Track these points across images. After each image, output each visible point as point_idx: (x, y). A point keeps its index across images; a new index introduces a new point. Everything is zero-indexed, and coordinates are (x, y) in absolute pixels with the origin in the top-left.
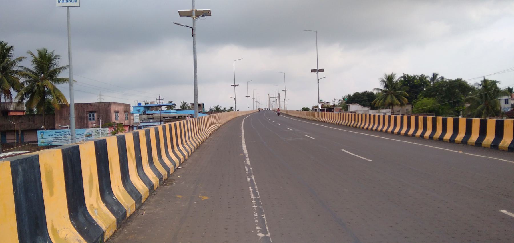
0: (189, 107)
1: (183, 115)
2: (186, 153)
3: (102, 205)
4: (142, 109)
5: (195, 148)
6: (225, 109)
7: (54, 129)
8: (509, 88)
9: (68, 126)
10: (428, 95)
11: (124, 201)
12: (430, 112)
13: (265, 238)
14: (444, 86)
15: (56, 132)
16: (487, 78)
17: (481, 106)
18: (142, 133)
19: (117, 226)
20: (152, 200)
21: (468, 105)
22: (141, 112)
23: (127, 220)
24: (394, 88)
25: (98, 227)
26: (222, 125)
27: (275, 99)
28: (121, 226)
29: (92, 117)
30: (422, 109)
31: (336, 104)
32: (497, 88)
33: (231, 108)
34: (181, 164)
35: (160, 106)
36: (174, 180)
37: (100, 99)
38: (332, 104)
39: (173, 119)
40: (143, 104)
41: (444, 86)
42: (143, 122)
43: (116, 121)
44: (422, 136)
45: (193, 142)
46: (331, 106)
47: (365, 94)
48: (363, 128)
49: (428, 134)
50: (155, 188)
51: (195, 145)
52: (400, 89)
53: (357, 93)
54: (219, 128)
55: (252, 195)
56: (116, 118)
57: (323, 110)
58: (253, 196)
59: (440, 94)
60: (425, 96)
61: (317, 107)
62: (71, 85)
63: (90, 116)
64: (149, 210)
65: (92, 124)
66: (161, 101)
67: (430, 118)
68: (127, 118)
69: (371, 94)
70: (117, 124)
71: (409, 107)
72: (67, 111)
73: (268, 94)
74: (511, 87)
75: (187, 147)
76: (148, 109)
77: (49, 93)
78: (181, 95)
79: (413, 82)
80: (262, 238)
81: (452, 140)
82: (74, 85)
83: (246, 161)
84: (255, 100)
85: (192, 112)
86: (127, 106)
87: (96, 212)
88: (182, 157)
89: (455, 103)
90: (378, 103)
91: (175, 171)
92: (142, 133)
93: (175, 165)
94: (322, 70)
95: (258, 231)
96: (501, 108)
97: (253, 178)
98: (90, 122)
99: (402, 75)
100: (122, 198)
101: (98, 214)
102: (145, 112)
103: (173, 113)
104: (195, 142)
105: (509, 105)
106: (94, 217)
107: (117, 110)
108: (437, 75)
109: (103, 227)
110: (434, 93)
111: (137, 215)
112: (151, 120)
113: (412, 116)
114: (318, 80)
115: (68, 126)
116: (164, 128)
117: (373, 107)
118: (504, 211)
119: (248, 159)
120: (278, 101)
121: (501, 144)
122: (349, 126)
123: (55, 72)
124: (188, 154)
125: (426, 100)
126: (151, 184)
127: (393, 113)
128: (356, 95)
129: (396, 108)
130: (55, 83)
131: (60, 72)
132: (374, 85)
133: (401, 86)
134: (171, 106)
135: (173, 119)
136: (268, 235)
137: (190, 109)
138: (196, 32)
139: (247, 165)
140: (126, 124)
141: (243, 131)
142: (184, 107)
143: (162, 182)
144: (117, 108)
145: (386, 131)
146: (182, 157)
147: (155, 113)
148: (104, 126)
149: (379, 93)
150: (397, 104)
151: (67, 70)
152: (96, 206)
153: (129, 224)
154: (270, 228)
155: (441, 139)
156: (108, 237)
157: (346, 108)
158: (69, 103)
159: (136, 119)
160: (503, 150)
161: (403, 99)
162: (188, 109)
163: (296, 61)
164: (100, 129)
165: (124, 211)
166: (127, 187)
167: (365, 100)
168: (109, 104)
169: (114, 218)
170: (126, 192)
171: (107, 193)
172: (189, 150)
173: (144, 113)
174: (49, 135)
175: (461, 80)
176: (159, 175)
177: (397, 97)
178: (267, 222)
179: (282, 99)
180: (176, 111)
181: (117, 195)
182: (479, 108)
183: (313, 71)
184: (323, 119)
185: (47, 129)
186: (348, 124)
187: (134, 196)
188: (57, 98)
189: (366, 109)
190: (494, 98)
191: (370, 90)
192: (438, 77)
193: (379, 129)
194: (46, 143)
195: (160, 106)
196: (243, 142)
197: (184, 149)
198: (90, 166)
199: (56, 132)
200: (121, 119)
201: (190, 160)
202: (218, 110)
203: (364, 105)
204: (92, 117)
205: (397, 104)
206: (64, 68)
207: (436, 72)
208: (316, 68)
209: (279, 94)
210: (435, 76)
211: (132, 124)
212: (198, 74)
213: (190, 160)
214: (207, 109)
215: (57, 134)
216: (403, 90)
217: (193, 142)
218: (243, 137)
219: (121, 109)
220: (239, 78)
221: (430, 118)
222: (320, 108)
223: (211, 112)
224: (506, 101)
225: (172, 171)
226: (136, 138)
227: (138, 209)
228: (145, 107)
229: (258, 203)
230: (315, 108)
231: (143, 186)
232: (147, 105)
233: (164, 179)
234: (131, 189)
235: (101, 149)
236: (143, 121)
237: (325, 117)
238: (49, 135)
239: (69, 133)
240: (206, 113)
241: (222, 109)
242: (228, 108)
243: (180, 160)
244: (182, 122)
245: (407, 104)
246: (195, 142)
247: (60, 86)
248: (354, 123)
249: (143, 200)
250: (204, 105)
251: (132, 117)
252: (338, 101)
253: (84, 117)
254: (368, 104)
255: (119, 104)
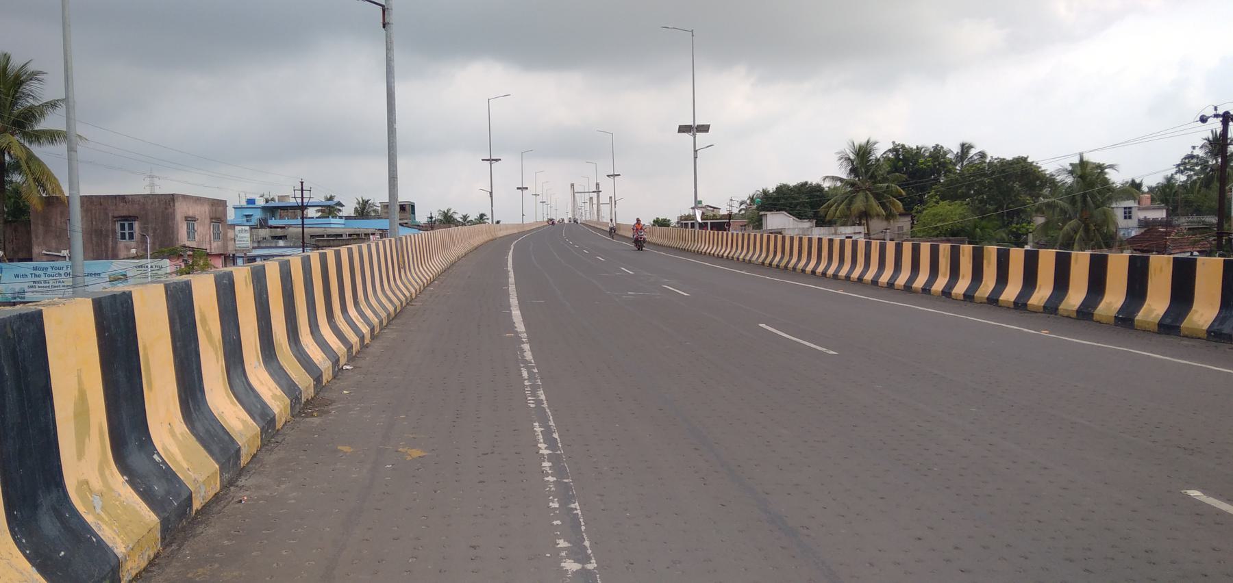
0: (376, 211)
1: (362, 231)
2: (365, 330)
3: (119, 482)
4: (258, 215)
5: (389, 315)
6: (465, 218)
7: (30, 260)
8: (1133, 181)
9: (65, 253)
10: (950, 194)
11: (185, 466)
12: (955, 234)
13: (584, 573)
14: (985, 175)
15: (35, 269)
16: (1086, 158)
17: (1073, 223)
18: (241, 274)
19: (163, 538)
20: (270, 458)
21: (1040, 220)
22: (254, 221)
23: (195, 517)
24: (873, 177)
25: (101, 547)
26: (459, 259)
27: (587, 196)
28: (174, 539)
29: (127, 231)
30: (937, 228)
31: (735, 211)
32: (1106, 181)
33: (482, 216)
34: (351, 358)
35: (303, 207)
36: (332, 402)
37: (152, 185)
38: (724, 212)
39: (336, 239)
40: (261, 202)
41: (985, 175)
42: (259, 247)
43: (188, 244)
44: (947, 293)
45: (384, 300)
46: (723, 217)
47: (804, 188)
48: (803, 271)
49: (961, 287)
50: (278, 426)
51: (391, 309)
52: (885, 180)
53: (785, 186)
54: (452, 265)
55: (542, 446)
56: (191, 234)
57: (703, 226)
58: (544, 450)
59: (978, 193)
60: (943, 198)
61: (692, 217)
62: (71, 149)
63: (123, 227)
64: (258, 487)
65: (128, 249)
66: (306, 194)
67: (966, 250)
68: (217, 236)
69: (818, 188)
70: (193, 249)
71: (905, 223)
72: (62, 213)
73: (572, 185)
74: (1138, 181)
75: (369, 313)
76: (273, 216)
77: (17, 167)
78: (357, 182)
79: (917, 161)
80: (573, 573)
81: (1020, 305)
82: (81, 149)
83: (522, 351)
84: (539, 199)
85: (384, 224)
86: (218, 206)
87: (98, 502)
88: (353, 339)
89: (1011, 215)
90: (833, 212)
91: (335, 377)
92: (241, 274)
93: (336, 362)
94: (704, 128)
95: (563, 554)
96: (1117, 228)
97: (543, 397)
98: (122, 244)
99: (891, 146)
100: (179, 457)
101: (103, 508)
102: (265, 220)
103: (336, 225)
104: (391, 301)
105: (1133, 223)
106: (89, 519)
107: (191, 214)
108: (970, 147)
109: (118, 544)
110: (964, 189)
111: (223, 503)
112: (281, 243)
113: (922, 244)
114: (696, 151)
115: (65, 253)
116: (323, 259)
117: (821, 222)
118: (1194, 493)
119: (526, 347)
120: (595, 201)
121: (1140, 316)
122: (770, 264)
123: (30, 115)
124: (372, 330)
125: (944, 207)
126: (268, 415)
127: (868, 235)
128: (782, 190)
129: (877, 225)
130: (31, 142)
131: (42, 114)
132: (824, 168)
133: (889, 173)
134: (330, 209)
135: (336, 239)
136: (592, 566)
137: (379, 217)
138: (393, 18)
139: (526, 362)
140: (214, 252)
141: (511, 274)
142: (363, 211)
143: (300, 406)
144: (192, 210)
145: (860, 279)
146: (353, 339)
147: (290, 226)
148: (158, 255)
149: (835, 188)
150: (878, 215)
151: (61, 110)
152: (96, 484)
153: (199, 530)
154: (594, 544)
155: (993, 300)
156: (134, 573)
157: (758, 223)
158: (67, 194)
159: (243, 237)
160: (1192, 336)
161: (892, 203)
162: (374, 218)
163: (643, 107)
164: (148, 262)
165: (184, 497)
166: (198, 425)
167: (803, 205)
168: (171, 199)
169: (151, 518)
170: (192, 440)
171: (133, 445)
172: (375, 321)
173: (263, 224)
174: (17, 276)
175: (1025, 159)
176: (290, 388)
177: (878, 197)
178: (586, 524)
179: (604, 198)
180: (342, 221)
181: (165, 449)
182: (1066, 227)
183: (683, 129)
184: (704, 248)
185: (11, 260)
186: (768, 261)
187: (215, 448)
188: (36, 180)
189: (806, 224)
190: (1103, 204)
191: (814, 179)
192: (973, 152)
193: (843, 273)
194: (9, 296)
195: (303, 207)
196: (514, 301)
197: (361, 319)
198: (79, 370)
199: (35, 269)
200: (203, 237)
201: (376, 347)
202: (448, 220)
203: (800, 216)
204: (127, 231)
205: (878, 215)
206: (53, 105)
207: (968, 140)
208: (690, 123)
209: (597, 185)
210: (965, 148)
211: (230, 250)
212: (398, 126)
213: (376, 347)
214: (421, 217)
215: (37, 272)
216: (893, 182)
217: (384, 300)
218: (512, 288)
219: (202, 211)
220: (505, 141)
221: (945, 248)
222: (699, 219)
223: (431, 225)
224: (1128, 214)
225: (327, 376)
226: (226, 290)
227: (227, 485)
228: (264, 208)
229: (559, 471)
230: (686, 222)
231: (244, 422)
232: (271, 204)
233: (304, 400)
234: (207, 431)
235: (116, 328)
236: (259, 243)
237: (708, 243)
238: (17, 276)
239: (69, 270)
240: (419, 227)
241: (458, 217)
242: (473, 216)
243: (349, 347)
244: (354, 247)
245: (901, 215)
246: (391, 301)
247: (42, 151)
248: (782, 258)
249: (244, 461)
250: (413, 207)
251: (231, 234)
252: (737, 205)
253: (107, 231)
254: (811, 214)
255: (198, 200)
